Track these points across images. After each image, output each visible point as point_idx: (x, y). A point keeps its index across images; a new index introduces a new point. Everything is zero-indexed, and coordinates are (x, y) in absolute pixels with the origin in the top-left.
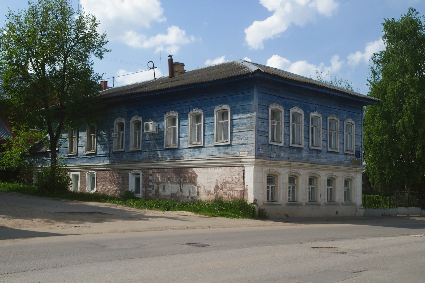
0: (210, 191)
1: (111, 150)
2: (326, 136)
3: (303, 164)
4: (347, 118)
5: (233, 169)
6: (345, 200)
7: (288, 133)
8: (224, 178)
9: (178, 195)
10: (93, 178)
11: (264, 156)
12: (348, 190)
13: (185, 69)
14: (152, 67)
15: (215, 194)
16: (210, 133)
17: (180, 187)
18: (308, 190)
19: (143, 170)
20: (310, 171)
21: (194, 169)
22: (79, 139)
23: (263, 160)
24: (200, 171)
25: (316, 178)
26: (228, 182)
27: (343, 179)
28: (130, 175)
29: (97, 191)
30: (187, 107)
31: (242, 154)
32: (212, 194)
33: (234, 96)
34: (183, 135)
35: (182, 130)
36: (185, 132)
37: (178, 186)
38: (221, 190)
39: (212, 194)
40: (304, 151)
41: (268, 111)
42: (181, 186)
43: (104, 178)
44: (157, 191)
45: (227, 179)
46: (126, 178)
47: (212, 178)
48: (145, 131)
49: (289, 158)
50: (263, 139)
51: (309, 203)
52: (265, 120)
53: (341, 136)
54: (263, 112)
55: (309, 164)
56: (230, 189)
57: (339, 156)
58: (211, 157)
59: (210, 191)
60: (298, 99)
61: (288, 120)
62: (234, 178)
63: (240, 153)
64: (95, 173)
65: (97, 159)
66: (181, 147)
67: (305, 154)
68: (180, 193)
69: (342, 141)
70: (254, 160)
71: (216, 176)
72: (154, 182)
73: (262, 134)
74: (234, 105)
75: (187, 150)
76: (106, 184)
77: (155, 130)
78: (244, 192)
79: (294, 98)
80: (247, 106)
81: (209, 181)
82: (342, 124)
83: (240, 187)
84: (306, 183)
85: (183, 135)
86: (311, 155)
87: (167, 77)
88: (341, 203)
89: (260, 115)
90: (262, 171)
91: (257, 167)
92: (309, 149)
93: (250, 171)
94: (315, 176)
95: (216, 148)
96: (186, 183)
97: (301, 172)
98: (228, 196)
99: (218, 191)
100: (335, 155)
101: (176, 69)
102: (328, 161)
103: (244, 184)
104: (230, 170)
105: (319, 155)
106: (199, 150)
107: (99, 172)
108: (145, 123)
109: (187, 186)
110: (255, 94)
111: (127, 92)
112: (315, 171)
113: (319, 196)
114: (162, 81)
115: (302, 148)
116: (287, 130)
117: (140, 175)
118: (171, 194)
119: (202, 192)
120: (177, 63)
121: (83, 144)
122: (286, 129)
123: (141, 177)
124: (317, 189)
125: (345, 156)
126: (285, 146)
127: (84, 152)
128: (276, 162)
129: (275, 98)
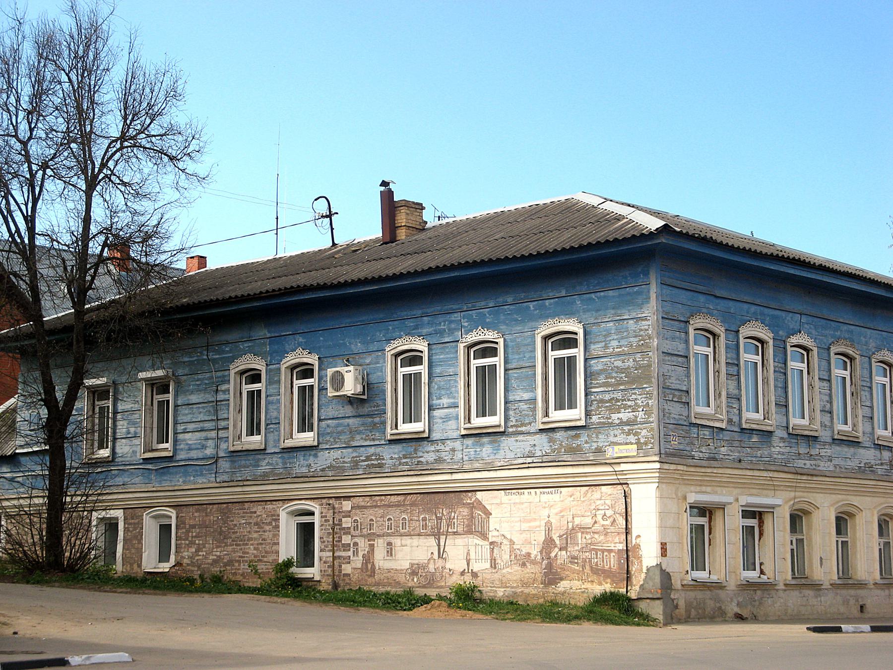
0: (529, 554)
1: (223, 446)
2: (827, 398)
3: (776, 475)
4: (879, 349)
5: (597, 493)
6: (881, 574)
7: (736, 392)
8: (570, 519)
9: (431, 567)
10: (165, 529)
11: (681, 456)
12: (887, 544)
13: (425, 219)
14: (325, 212)
15: (545, 562)
16: (526, 396)
17: (439, 545)
18: (789, 547)
19: (324, 501)
20: (792, 494)
21: (479, 495)
22: (119, 416)
23: (680, 467)
24: (498, 501)
25: (807, 513)
26: (583, 529)
27: (873, 515)
28: (283, 516)
29: (178, 564)
30: (453, 326)
31: (621, 451)
32: (534, 562)
33: (593, 296)
34: (445, 401)
35: (439, 388)
36: (450, 395)
37: (432, 541)
38: (560, 550)
39: (534, 562)
40: (775, 440)
41: (687, 333)
42: (442, 544)
43: (203, 525)
44: (368, 559)
45: (577, 521)
46: (270, 524)
47: (535, 520)
48: (331, 393)
49: (740, 461)
50: (676, 410)
51: (794, 582)
52: (680, 359)
53: (864, 398)
54: (673, 339)
55: (790, 476)
56: (589, 547)
57: (861, 451)
58: (529, 460)
59: (529, 554)
60: (758, 301)
61: (735, 356)
62: (599, 518)
63: (616, 448)
64: (173, 513)
65: (176, 473)
66: (436, 436)
67: (778, 448)
68: (440, 563)
69: (867, 411)
70: (657, 465)
71: (545, 512)
72: (357, 533)
73: (674, 396)
74: (592, 321)
75: (457, 445)
76: (206, 542)
77: (359, 389)
78: (629, 554)
79: (749, 300)
80: (631, 322)
81: (525, 526)
82: (867, 365)
83: (617, 540)
84: (784, 528)
85: (445, 401)
86: (794, 450)
87: (376, 240)
88: (872, 582)
89: (668, 346)
90: (676, 495)
91: (664, 486)
92: (789, 434)
93: (647, 499)
94: (806, 507)
95: (544, 437)
96: (455, 533)
97: (819, 499)
98: (584, 567)
99: (553, 555)
100: (852, 450)
101: (402, 218)
102: (835, 466)
103: (627, 531)
104: (586, 494)
105: (814, 452)
106: (491, 442)
107: (185, 509)
108: (330, 372)
109: (460, 541)
110: (653, 289)
111: (270, 285)
112: (805, 494)
113: (816, 562)
114: (354, 251)
115: (770, 433)
116: (732, 385)
117: (312, 514)
118: (412, 565)
119: (506, 557)
120: (407, 204)
121: (132, 430)
122: (730, 382)
123: (317, 520)
124: (810, 544)
125: (878, 452)
126: (729, 428)
127: (134, 452)
128: (709, 470)
129: (702, 298)
